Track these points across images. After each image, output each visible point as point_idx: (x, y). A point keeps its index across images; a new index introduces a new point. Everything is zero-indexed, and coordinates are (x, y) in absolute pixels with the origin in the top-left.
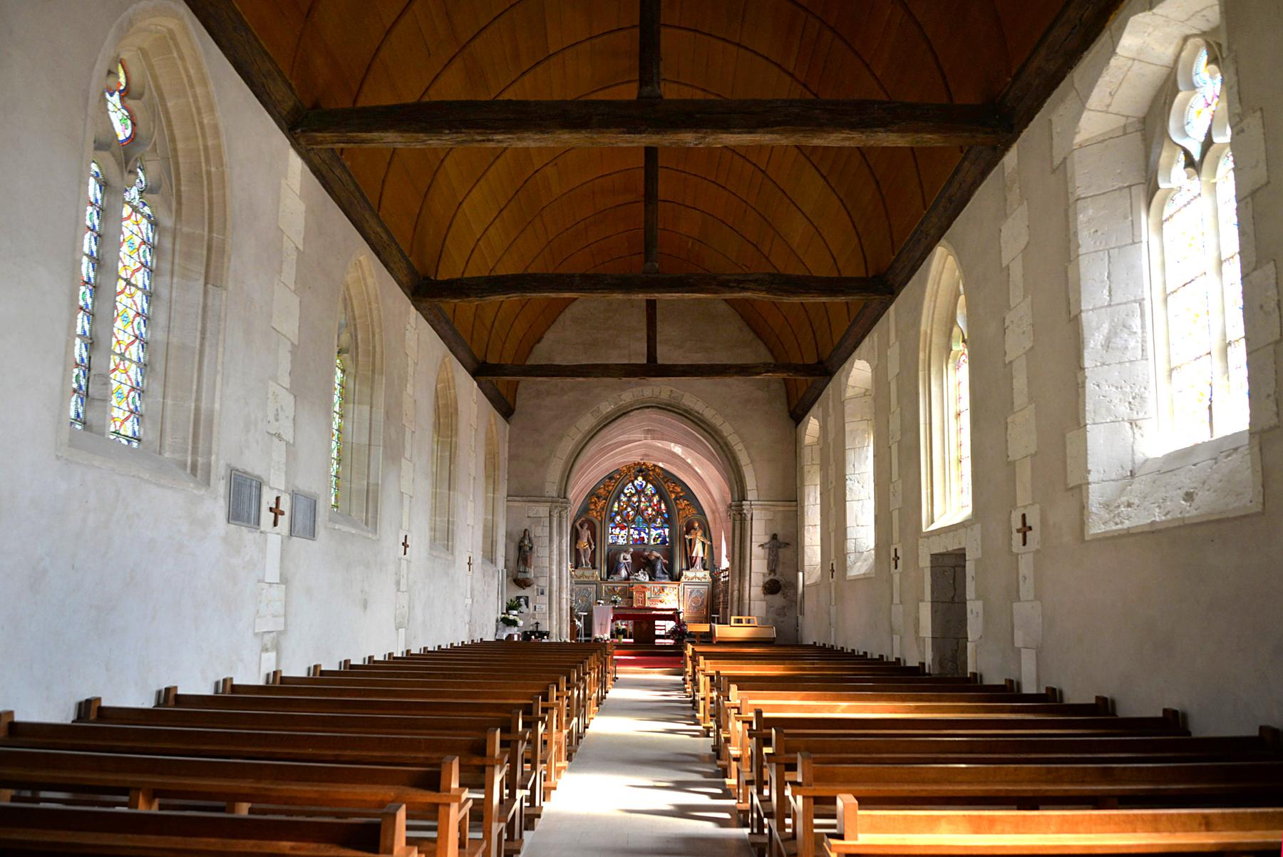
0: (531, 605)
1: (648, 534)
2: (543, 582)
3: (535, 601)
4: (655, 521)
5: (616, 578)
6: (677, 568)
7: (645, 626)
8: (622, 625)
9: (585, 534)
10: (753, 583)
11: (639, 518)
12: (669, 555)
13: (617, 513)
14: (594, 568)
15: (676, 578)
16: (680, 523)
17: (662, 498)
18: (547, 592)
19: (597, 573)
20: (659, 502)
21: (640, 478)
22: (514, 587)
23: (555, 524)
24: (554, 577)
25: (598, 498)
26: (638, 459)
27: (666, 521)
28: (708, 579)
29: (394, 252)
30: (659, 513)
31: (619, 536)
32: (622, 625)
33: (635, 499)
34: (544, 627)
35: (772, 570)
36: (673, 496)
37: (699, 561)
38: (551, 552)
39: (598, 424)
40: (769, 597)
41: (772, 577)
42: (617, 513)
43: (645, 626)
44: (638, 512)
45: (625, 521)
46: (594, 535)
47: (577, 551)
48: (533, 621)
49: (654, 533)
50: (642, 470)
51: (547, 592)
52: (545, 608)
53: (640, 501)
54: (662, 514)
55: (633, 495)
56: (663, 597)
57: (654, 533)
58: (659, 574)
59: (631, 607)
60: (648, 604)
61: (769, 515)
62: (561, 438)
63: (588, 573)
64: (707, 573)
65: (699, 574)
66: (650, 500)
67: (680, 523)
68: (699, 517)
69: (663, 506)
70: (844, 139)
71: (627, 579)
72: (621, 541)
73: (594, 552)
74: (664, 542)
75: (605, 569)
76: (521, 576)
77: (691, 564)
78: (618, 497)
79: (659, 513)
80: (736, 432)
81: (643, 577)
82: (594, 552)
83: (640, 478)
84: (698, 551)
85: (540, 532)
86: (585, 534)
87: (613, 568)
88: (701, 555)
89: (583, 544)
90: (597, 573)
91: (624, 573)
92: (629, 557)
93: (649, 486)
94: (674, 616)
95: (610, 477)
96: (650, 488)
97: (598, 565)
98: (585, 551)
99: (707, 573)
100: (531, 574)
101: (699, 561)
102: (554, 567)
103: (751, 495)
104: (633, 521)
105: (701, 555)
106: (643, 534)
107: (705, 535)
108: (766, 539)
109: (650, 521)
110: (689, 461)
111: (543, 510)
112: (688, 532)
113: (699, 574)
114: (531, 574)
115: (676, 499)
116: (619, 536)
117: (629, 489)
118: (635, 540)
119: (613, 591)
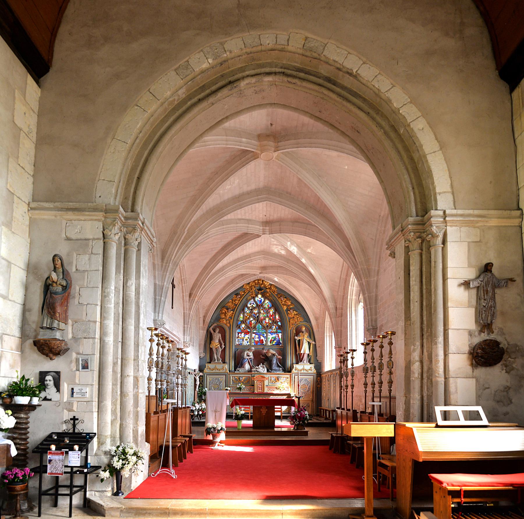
0: (65, 387)
1: (266, 337)
2: (89, 348)
3: (72, 381)
4: (271, 328)
5: (241, 370)
6: (289, 363)
7: (264, 411)
8: (240, 411)
9: (217, 336)
10: (452, 347)
11: (259, 326)
12: (283, 353)
13: (243, 322)
14: (224, 362)
15: (288, 370)
16: (291, 329)
17: (277, 310)
18: (95, 365)
19: (226, 366)
20: (275, 313)
21: (260, 296)
22: (35, 355)
23: (113, 251)
24: (110, 339)
25: (227, 309)
26: (258, 274)
27: (280, 328)
28: (314, 371)
29: (114, 187)
30: (274, 322)
31: (243, 339)
32: (240, 411)
33: (256, 311)
34: (89, 424)
35: (485, 326)
36: (285, 308)
37: (306, 357)
38: (104, 296)
39: (189, 97)
40: (481, 371)
41: (485, 336)
42: (243, 322)
43: (264, 411)
44: (258, 320)
45: (248, 328)
46: (224, 338)
47: (211, 349)
48: (67, 416)
49: (270, 337)
50: (260, 288)
51: (95, 365)
52: (91, 392)
53: (259, 313)
54: (276, 323)
55: (254, 308)
56: (278, 384)
57: (270, 337)
58: (274, 367)
59: (253, 393)
60: (266, 390)
61: (475, 235)
62: (124, 108)
63: (220, 366)
64: (312, 366)
65: (305, 368)
66: (268, 312)
67: (291, 329)
68: (305, 323)
69: (277, 317)
70: (97, 359)
71: (250, 371)
72: (245, 343)
73: (224, 351)
74: (278, 343)
75: (232, 364)
76: (44, 335)
77: (299, 359)
78: (243, 310)
79: (274, 322)
80: (413, 101)
81: (262, 369)
82: (224, 351)
83: (260, 296)
84: (305, 349)
85: (85, 266)
86: (217, 336)
87: (239, 363)
88: (307, 352)
89: (215, 343)
90: (226, 366)
91: (247, 367)
92: (251, 354)
93: (267, 301)
94: (289, 402)
95: (236, 293)
96: (267, 303)
97: (227, 360)
98: (217, 349)
99: (312, 366)
100: (65, 332)
101: (306, 357)
102: (110, 324)
103: (444, 202)
104: (255, 328)
105: (307, 352)
106: (262, 338)
107: (310, 336)
108: (470, 274)
109: (266, 328)
110: (303, 261)
111: (90, 227)
112: (297, 334)
113: (305, 368)
114: (65, 332)
115: (288, 310)
116: (243, 339)
117: (251, 304)
118: (256, 342)
119: (239, 380)
